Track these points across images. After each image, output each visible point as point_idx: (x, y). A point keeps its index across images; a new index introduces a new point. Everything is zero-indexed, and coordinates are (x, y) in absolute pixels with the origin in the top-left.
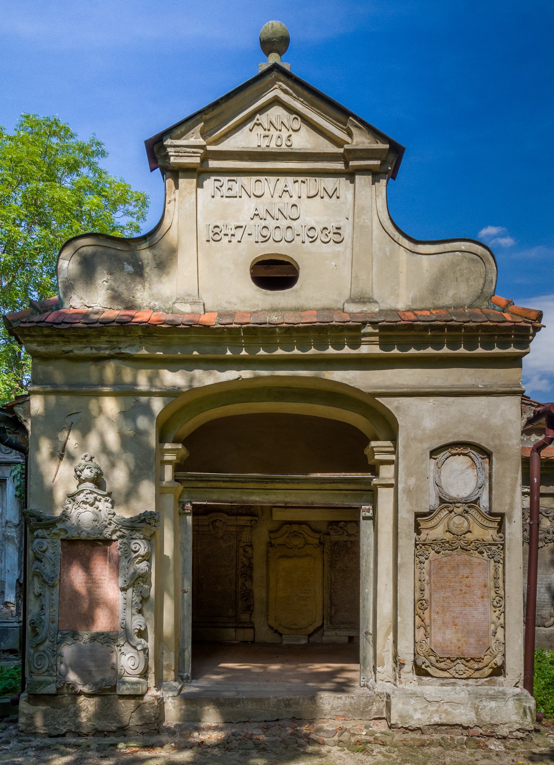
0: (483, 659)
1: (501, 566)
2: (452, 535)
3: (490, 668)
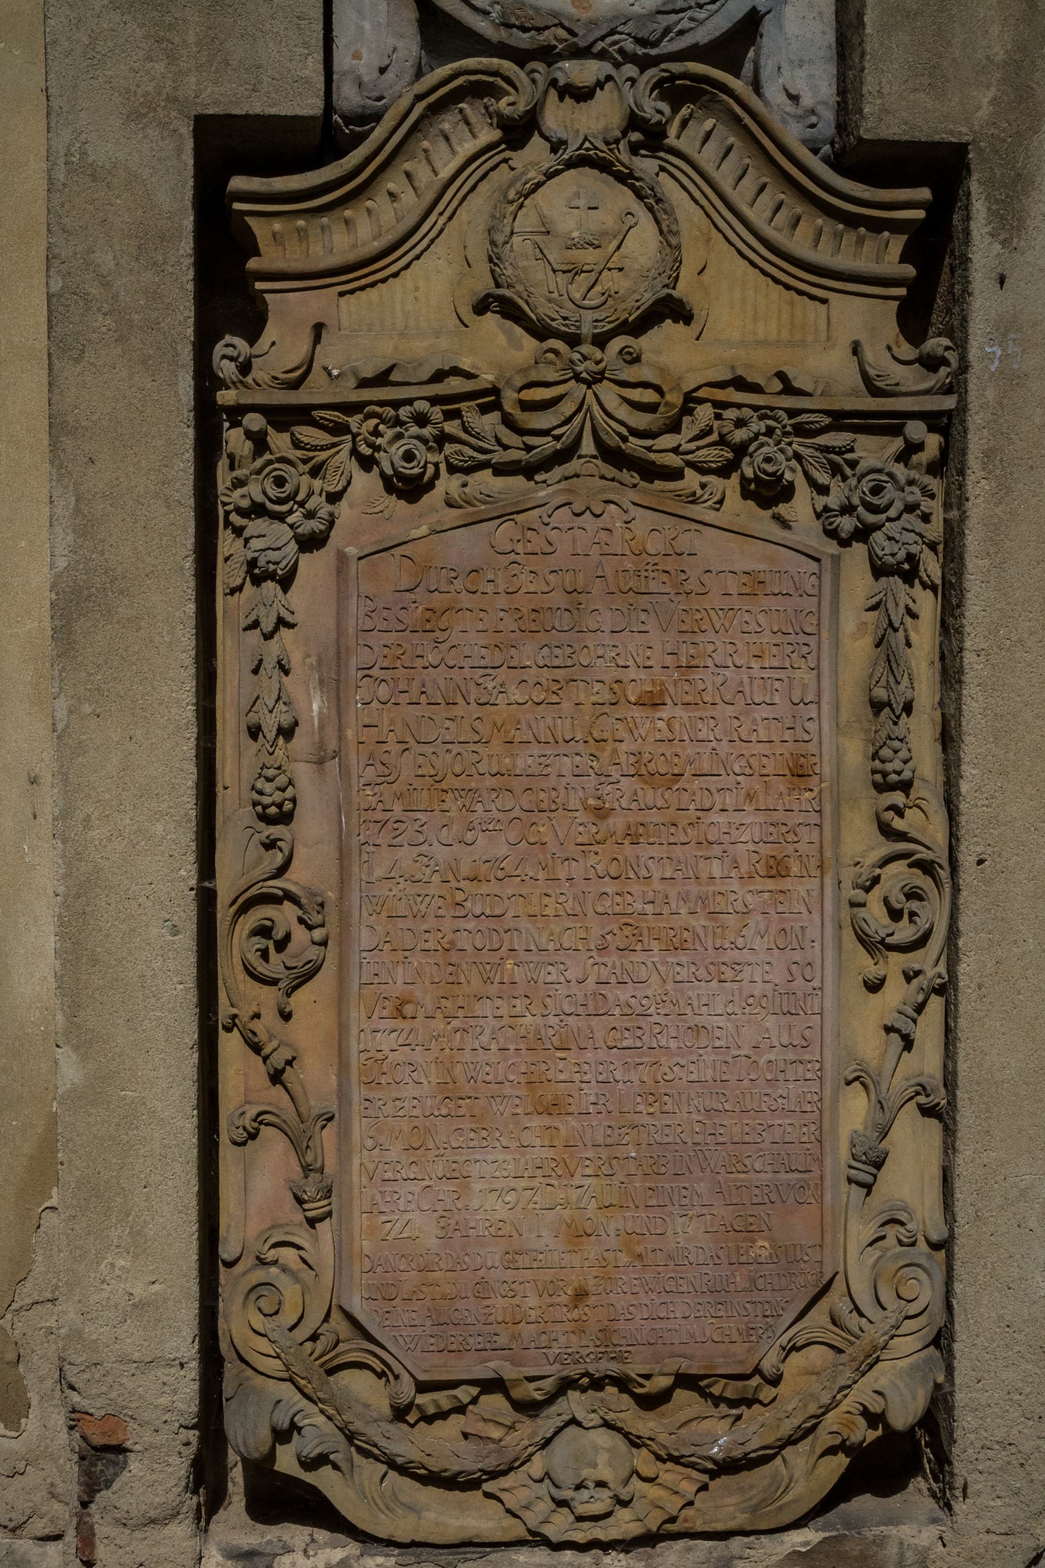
0: (775, 1381)
1: (927, 604)
2: (530, 344)
3: (831, 1451)
